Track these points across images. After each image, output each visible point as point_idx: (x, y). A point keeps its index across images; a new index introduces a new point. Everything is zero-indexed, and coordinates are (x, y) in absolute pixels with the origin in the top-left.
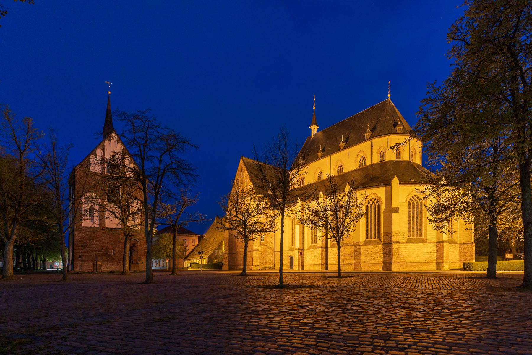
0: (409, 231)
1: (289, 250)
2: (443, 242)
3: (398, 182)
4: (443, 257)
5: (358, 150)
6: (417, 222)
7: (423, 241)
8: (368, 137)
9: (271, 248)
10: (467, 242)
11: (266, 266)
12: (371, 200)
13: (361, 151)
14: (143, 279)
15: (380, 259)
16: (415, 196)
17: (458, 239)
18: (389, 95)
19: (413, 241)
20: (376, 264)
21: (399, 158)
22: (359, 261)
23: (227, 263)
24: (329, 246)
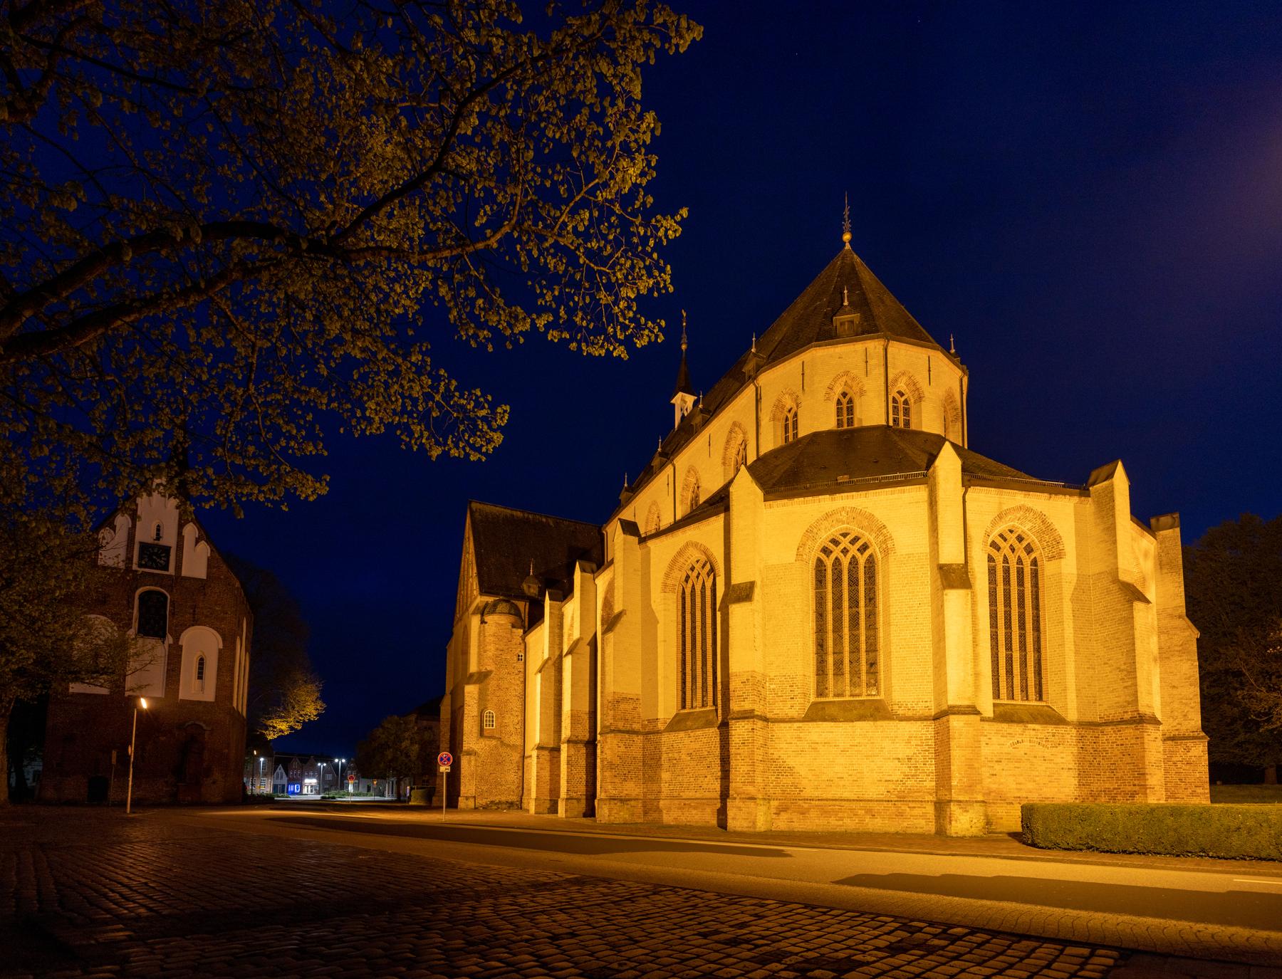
0: (821, 670)
3: (760, 493)
6: (854, 639)
7: (877, 712)
9: (513, 747)
10: (1115, 714)
11: (497, 799)
12: (692, 569)
16: (845, 535)
17: (1072, 696)
18: (847, 237)
19: (833, 711)
21: (850, 421)
22: (655, 787)
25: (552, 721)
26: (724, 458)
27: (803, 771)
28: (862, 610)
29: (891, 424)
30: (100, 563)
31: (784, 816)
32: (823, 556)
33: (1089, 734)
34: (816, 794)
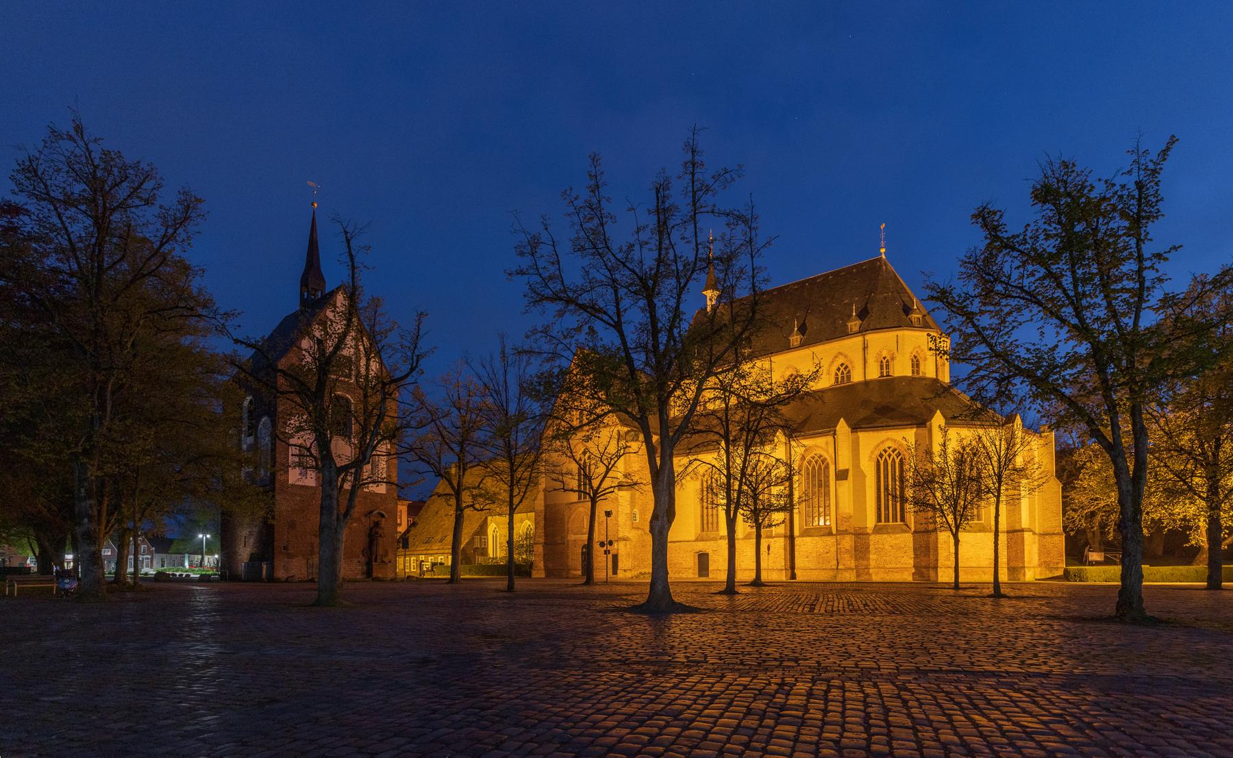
1: (696, 540)
2: (1022, 531)
4: (1023, 558)
5: (835, 352)
8: (856, 329)
13: (840, 353)
14: (723, 587)
15: (908, 560)
18: (883, 250)
20: (901, 570)
23: (541, 564)
24: (796, 533)
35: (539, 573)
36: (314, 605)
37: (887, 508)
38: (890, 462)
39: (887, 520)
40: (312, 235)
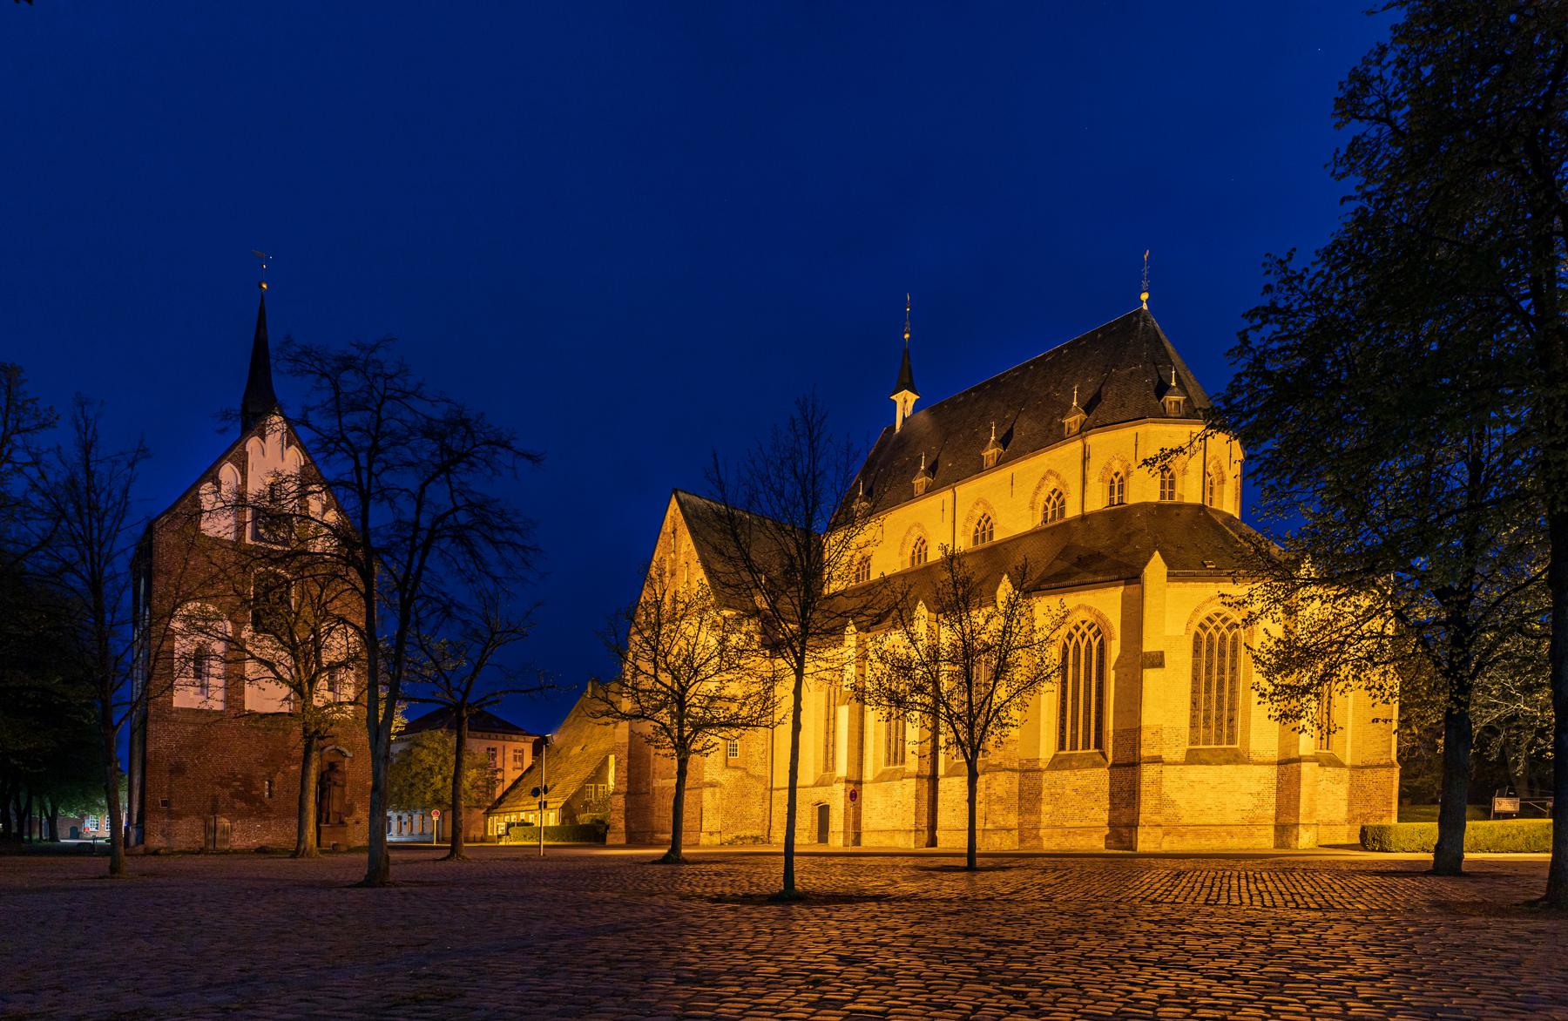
1: (816, 785)
2: (1299, 760)
4: (1298, 808)
6: (1220, 698)
8: (1075, 429)
9: (758, 778)
10: (1374, 760)
13: (1050, 472)
14: (360, 874)
16: (1218, 615)
18: (1145, 296)
19: (1204, 756)
20: (1087, 830)
21: (1171, 496)
22: (1034, 818)
23: (622, 825)
24: (941, 771)
25: (856, 755)
26: (1033, 503)
27: (1182, 803)
28: (1227, 677)
29: (1207, 503)
30: (231, 537)
31: (1167, 839)
32: (1200, 631)
33: (1355, 774)
34: (1190, 821)
35: (617, 834)
36: (360, 885)
37: (1075, 725)
38: (1083, 646)
39: (1074, 747)
40: (257, 334)
